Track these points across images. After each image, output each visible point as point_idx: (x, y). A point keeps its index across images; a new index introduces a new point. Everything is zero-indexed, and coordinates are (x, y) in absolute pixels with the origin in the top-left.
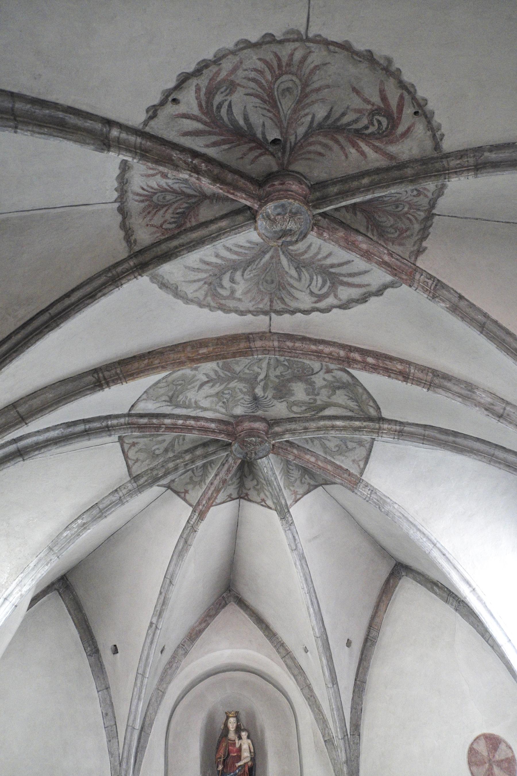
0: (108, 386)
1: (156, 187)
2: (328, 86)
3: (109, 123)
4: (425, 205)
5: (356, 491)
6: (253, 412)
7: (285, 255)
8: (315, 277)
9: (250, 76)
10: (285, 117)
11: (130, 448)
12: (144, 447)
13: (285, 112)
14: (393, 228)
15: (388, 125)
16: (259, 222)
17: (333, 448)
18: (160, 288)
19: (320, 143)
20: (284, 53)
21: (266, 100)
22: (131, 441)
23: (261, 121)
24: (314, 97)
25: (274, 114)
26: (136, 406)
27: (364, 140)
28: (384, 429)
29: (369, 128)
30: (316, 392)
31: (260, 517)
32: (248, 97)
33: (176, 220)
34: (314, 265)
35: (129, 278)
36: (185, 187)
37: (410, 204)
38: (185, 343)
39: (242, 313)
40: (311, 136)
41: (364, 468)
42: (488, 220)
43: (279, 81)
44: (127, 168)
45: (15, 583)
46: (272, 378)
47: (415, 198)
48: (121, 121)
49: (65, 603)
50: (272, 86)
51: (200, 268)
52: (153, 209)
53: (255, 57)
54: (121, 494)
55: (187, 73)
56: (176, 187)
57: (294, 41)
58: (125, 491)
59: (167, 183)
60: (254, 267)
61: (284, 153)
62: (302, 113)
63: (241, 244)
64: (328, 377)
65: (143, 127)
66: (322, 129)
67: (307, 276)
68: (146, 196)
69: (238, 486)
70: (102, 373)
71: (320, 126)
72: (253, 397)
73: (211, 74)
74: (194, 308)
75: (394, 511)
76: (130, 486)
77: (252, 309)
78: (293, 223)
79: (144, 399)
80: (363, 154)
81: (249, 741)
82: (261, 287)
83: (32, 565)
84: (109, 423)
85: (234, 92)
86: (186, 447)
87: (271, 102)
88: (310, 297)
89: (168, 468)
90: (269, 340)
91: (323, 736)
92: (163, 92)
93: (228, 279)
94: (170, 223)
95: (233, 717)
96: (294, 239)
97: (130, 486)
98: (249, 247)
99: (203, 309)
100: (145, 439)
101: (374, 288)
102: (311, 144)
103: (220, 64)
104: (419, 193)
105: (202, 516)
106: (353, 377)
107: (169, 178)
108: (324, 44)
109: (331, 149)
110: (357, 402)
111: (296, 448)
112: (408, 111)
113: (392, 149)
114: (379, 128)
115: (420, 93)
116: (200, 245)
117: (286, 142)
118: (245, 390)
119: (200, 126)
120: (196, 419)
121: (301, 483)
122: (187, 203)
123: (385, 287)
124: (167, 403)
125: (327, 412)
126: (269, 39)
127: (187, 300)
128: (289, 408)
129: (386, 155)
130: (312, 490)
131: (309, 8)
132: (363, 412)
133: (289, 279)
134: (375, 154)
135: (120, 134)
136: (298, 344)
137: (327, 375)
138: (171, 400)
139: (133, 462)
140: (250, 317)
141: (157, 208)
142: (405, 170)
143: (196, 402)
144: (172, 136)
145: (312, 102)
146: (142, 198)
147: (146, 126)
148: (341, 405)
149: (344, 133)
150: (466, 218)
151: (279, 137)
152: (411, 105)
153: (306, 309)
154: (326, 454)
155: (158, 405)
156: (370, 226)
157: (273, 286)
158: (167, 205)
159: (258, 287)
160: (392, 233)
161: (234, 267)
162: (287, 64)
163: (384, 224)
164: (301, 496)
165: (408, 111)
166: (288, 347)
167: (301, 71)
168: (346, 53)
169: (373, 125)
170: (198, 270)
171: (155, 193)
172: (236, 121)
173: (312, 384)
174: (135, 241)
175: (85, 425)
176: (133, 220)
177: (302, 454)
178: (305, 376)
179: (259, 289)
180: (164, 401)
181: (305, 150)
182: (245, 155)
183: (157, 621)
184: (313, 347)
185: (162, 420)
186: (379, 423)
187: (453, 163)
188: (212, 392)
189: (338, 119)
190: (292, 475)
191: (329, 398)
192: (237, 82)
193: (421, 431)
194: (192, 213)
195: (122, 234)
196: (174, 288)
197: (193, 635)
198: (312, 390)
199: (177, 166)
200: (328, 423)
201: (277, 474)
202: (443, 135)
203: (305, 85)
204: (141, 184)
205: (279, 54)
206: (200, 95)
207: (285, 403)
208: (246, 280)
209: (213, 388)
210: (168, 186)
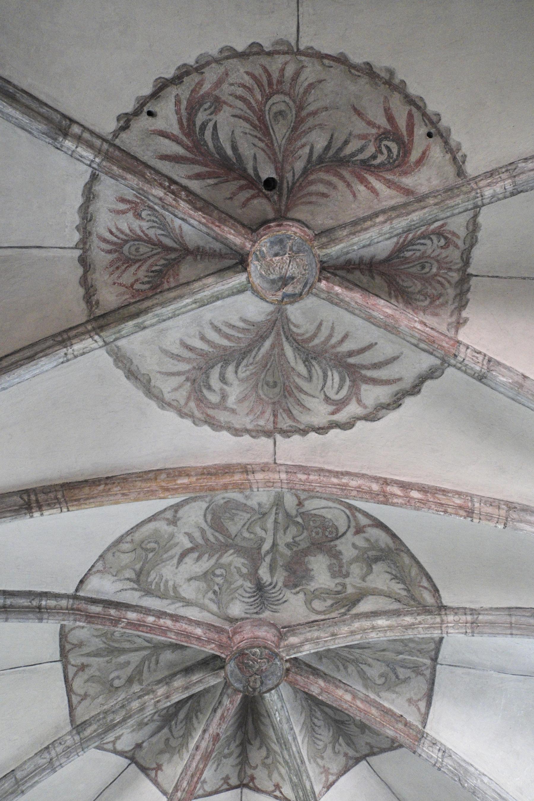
2: (326, 109)
5: (419, 751)
6: (257, 613)
8: (329, 373)
9: (238, 93)
10: (280, 147)
11: (75, 674)
12: (97, 673)
13: (279, 141)
14: (423, 295)
15: (399, 152)
17: (377, 679)
18: (128, 378)
21: (256, 125)
23: (252, 152)
24: (311, 122)
25: (267, 145)
26: (86, 582)
27: (372, 173)
28: (448, 623)
29: (377, 157)
30: (344, 572)
32: (236, 119)
33: (150, 279)
34: (327, 355)
35: (83, 337)
36: (163, 235)
37: (438, 261)
38: (158, 470)
39: (237, 432)
40: (311, 174)
41: (427, 714)
43: (270, 102)
44: (92, 196)
46: (282, 548)
47: (443, 251)
52: (123, 264)
53: (242, 70)
55: (166, 79)
56: (152, 233)
57: (284, 53)
58: (59, 749)
60: (251, 360)
61: (280, 196)
62: (299, 144)
63: (233, 323)
64: (359, 541)
68: (115, 244)
69: (239, 760)
70: (36, 495)
71: (321, 160)
72: (257, 585)
74: (171, 416)
76: (69, 740)
77: (249, 427)
79: (98, 571)
80: (373, 190)
82: (260, 392)
84: (43, 603)
85: (220, 110)
87: (263, 128)
88: (325, 406)
89: (131, 709)
90: (274, 471)
92: (138, 99)
94: (143, 283)
97: (69, 740)
98: (243, 329)
99: (184, 420)
101: (407, 384)
102: (311, 183)
103: (202, 73)
108: (318, 58)
109: (335, 188)
111: (322, 677)
112: (420, 131)
113: (408, 181)
114: (389, 155)
115: (432, 107)
117: (282, 183)
118: (244, 571)
119: (180, 151)
120: (176, 618)
121: (335, 752)
123: (423, 379)
126: (255, 50)
127: (164, 403)
128: (308, 602)
129: (401, 190)
130: (352, 767)
131: (298, 16)
134: (388, 190)
135: (82, 133)
137: (357, 537)
139: (79, 699)
140: (247, 438)
141: (128, 263)
142: (427, 200)
143: (175, 588)
144: (147, 157)
146: (109, 247)
147: (117, 137)
148: (382, 590)
149: (349, 166)
150: (511, 278)
151: (274, 176)
152: (423, 123)
153: (321, 425)
154: (367, 689)
155: (119, 586)
156: (392, 292)
157: (277, 390)
159: (257, 392)
160: (422, 301)
162: (278, 81)
163: (410, 290)
164: (334, 778)
166: (300, 479)
168: (342, 67)
169: (382, 153)
171: (126, 242)
173: (336, 555)
174: (97, 303)
175: (5, 598)
176: (97, 275)
177: (331, 688)
180: (128, 579)
181: (305, 191)
182: (234, 194)
184: (335, 480)
185: (124, 612)
186: (440, 615)
188: (198, 570)
189: (341, 149)
190: (318, 736)
191: (364, 580)
194: (171, 272)
195: (81, 291)
196: (145, 381)
198: (338, 571)
203: (300, 108)
204: (109, 224)
208: (242, 380)
209: (200, 563)
210: (143, 231)
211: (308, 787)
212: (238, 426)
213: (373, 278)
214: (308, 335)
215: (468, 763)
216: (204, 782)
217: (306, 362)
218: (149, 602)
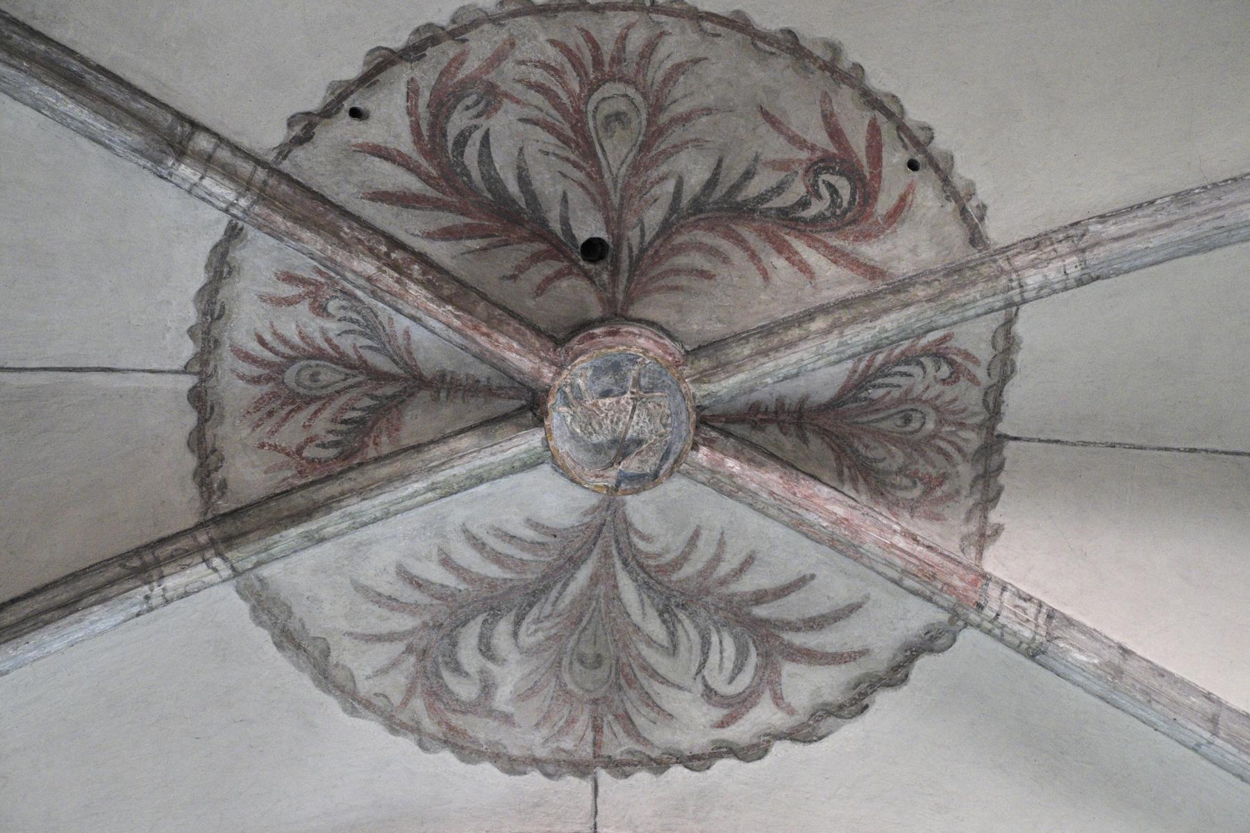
1: (296, 340)
2: (708, 111)
4: (977, 409)
7: (630, 573)
8: (715, 639)
9: (533, 79)
10: (615, 182)
13: (614, 171)
14: (906, 476)
15: (853, 195)
16: (554, 420)
18: (279, 646)
19: (700, 247)
20: (606, 34)
21: (568, 138)
25: (588, 175)
27: (801, 234)
29: (810, 203)
33: (339, 438)
34: (709, 599)
36: (370, 348)
37: (936, 409)
39: (513, 765)
40: (678, 232)
42: (1141, 448)
43: (597, 96)
44: (226, 270)
47: (947, 388)
50: (582, 107)
51: (396, 595)
52: (283, 404)
53: (542, 38)
55: (391, 51)
59: (324, 332)
60: (548, 609)
61: (615, 274)
62: (654, 174)
65: (277, 158)
66: (701, 211)
67: (694, 635)
71: (697, 206)
73: (445, 61)
74: (371, 728)
77: (541, 753)
78: (644, 416)
80: (804, 268)
82: (566, 678)
87: (580, 143)
88: (705, 708)
92: (332, 87)
93: (474, 642)
94: (323, 446)
98: (532, 543)
99: (400, 739)
101: (880, 661)
102: (679, 250)
107: (329, 315)
108: (691, 18)
109: (726, 260)
112: (894, 158)
113: (872, 251)
114: (833, 201)
115: (915, 115)
116: (397, 484)
117: (618, 245)
119: (413, 184)
122: (373, 397)
123: (912, 652)
133: (646, 651)
135: (215, 150)
140: (534, 780)
141: (292, 403)
144: (345, 194)
145: (675, 146)
146: (256, 371)
147: (285, 157)
149: (753, 220)
150: (1085, 444)
151: (603, 235)
152: (899, 144)
153: (696, 751)
156: (846, 470)
157: (601, 673)
158: (320, 398)
159: (558, 677)
160: (906, 488)
161: (495, 603)
162: (613, 59)
163: (881, 465)
167: (645, 75)
168: (739, 36)
169: (820, 197)
170: (391, 602)
171: (292, 360)
172: (499, 181)
174: (224, 485)
176: (225, 429)
179: (562, 686)
181: (666, 266)
182: (521, 269)
189: (737, 187)
192: (503, 88)
194: (383, 424)
195: (191, 462)
196: (316, 654)
202: (983, 208)
203: (657, 108)
204: (258, 325)
205: (594, 34)
206: (416, 106)
208: (528, 652)
210: (328, 340)
212: (515, 752)
214: (669, 557)
217: (665, 612)
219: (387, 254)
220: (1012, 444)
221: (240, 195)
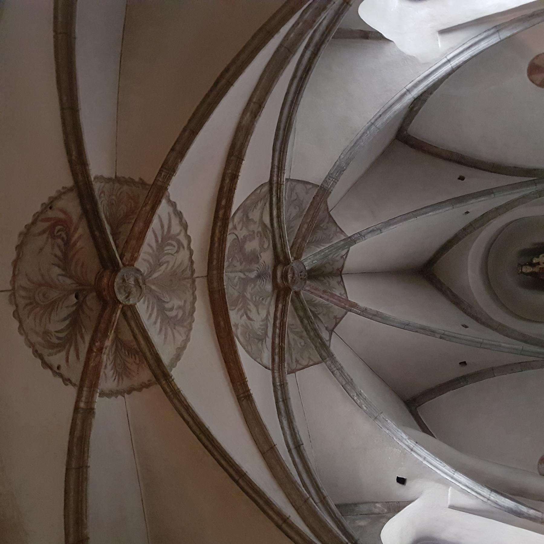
0: (249, 390)
1: (113, 371)
2: (40, 269)
3: (76, 409)
8: (166, 252)
11: (300, 364)
15: (60, 225)
18: (180, 360)
22: (294, 364)
31: (357, 256)
39: (195, 298)
45: (400, 443)
48: (74, 401)
49: (426, 401)
54: (335, 369)
57: (15, 298)
58: (333, 366)
59: (110, 365)
67: (165, 257)
75: (346, 158)
76: (329, 362)
77: (191, 292)
79: (261, 360)
81: (541, 256)
83: (387, 431)
84: (278, 384)
86: (299, 322)
87: (53, 305)
91: (537, 198)
93: (170, 312)
94: (136, 359)
95: (522, 269)
96: (140, 277)
97: (329, 362)
100: (293, 353)
101: (171, 209)
104: (103, 192)
105: (354, 305)
106: (238, 209)
110: (258, 202)
112: (50, 214)
113: (75, 218)
114: (62, 231)
115: (39, 209)
122: (121, 349)
123: (169, 201)
124: (264, 343)
125: (267, 221)
126: (16, 314)
127: (188, 339)
128: (265, 250)
132: (265, 196)
133: (168, 269)
136: (215, 256)
138: (261, 340)
140: (197, 293)
144: (80, 367)
155: (265, 349)
161: (162, 310)
164: (338, 228)
165: (50, 214)
169: (61, 235)
171: (117, 371)
172: (67, 325)
173: (245, 237)
174: (149, 381)
178: (240, 244)
183: (439, 334)
184: (216, 245)
187: (80, 177)
193: (277, 154)
195: (144, 390)
197: (457, 301)
198: (251, 236)
199: (99, 362)
200: (275, 220)
201: (319, 250)
202: (63, 188)
203: (40, 285)
207: (262, 254)
211: (342, 243)
212: (192, 298)
213: (120, 232)
214: (148, 265)
215: (335, 165)
216: (340, 294)
217: (160, 265)
218: (270, 334)
219: (95, 352)
220: (117, 174)
221: (97, 392)
